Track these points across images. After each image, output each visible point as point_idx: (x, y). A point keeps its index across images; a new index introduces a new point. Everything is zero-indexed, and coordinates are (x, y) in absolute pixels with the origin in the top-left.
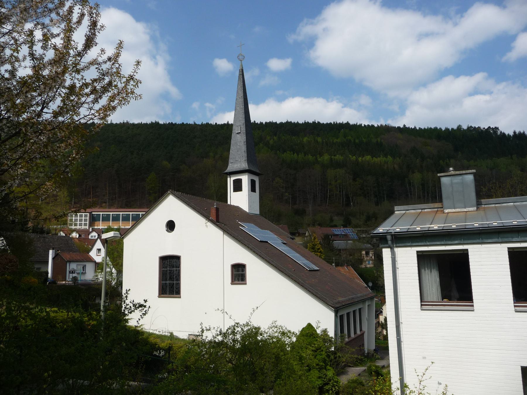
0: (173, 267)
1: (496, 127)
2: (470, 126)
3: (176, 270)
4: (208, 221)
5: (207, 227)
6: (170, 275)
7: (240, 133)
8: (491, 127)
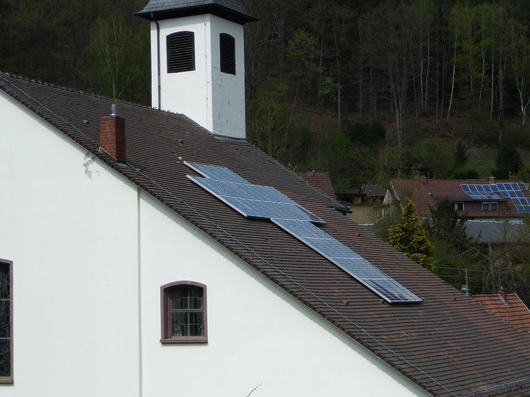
4: (93, 159)
5: (90, 177)
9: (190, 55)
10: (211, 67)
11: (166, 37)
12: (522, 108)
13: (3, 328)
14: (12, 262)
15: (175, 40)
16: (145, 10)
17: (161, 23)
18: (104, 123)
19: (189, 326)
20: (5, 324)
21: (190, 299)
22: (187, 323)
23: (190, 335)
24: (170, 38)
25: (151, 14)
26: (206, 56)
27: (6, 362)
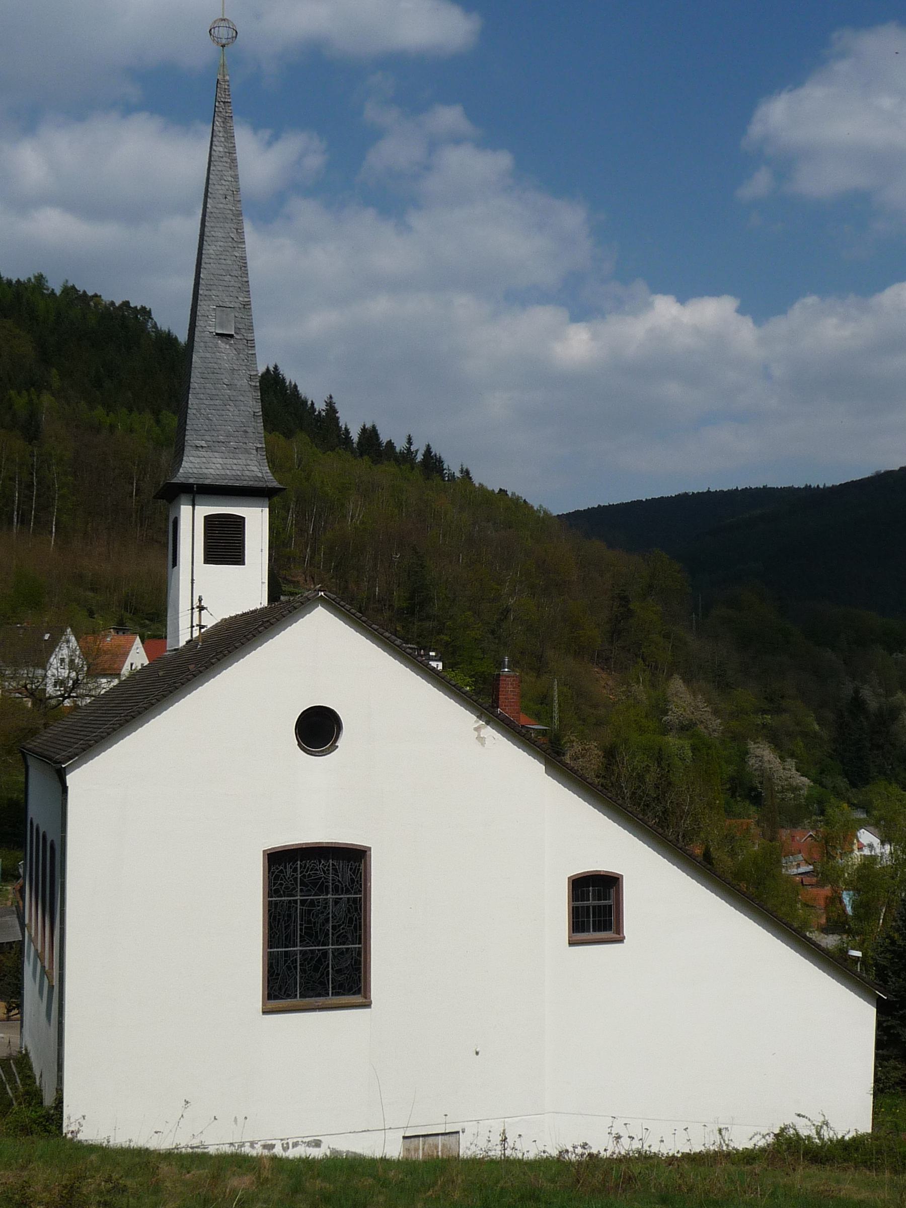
0: (323, 889)
1: (143, 308)
2: (70, 284)
3: (336, 902)
4: (488, 723)
5: (483, 744)
6: (309, 922)
7: (231, 336)
8: (132, 305)
13: (343, 933)
14: (370, 848)
17: (197, 498)
18: (505, 680)
19: (591, 922)
20: (346, 928)
21: (593, 890)
22: (590, 918)
23: (593, 931)
24: (209, 520)
27: (347, 977)
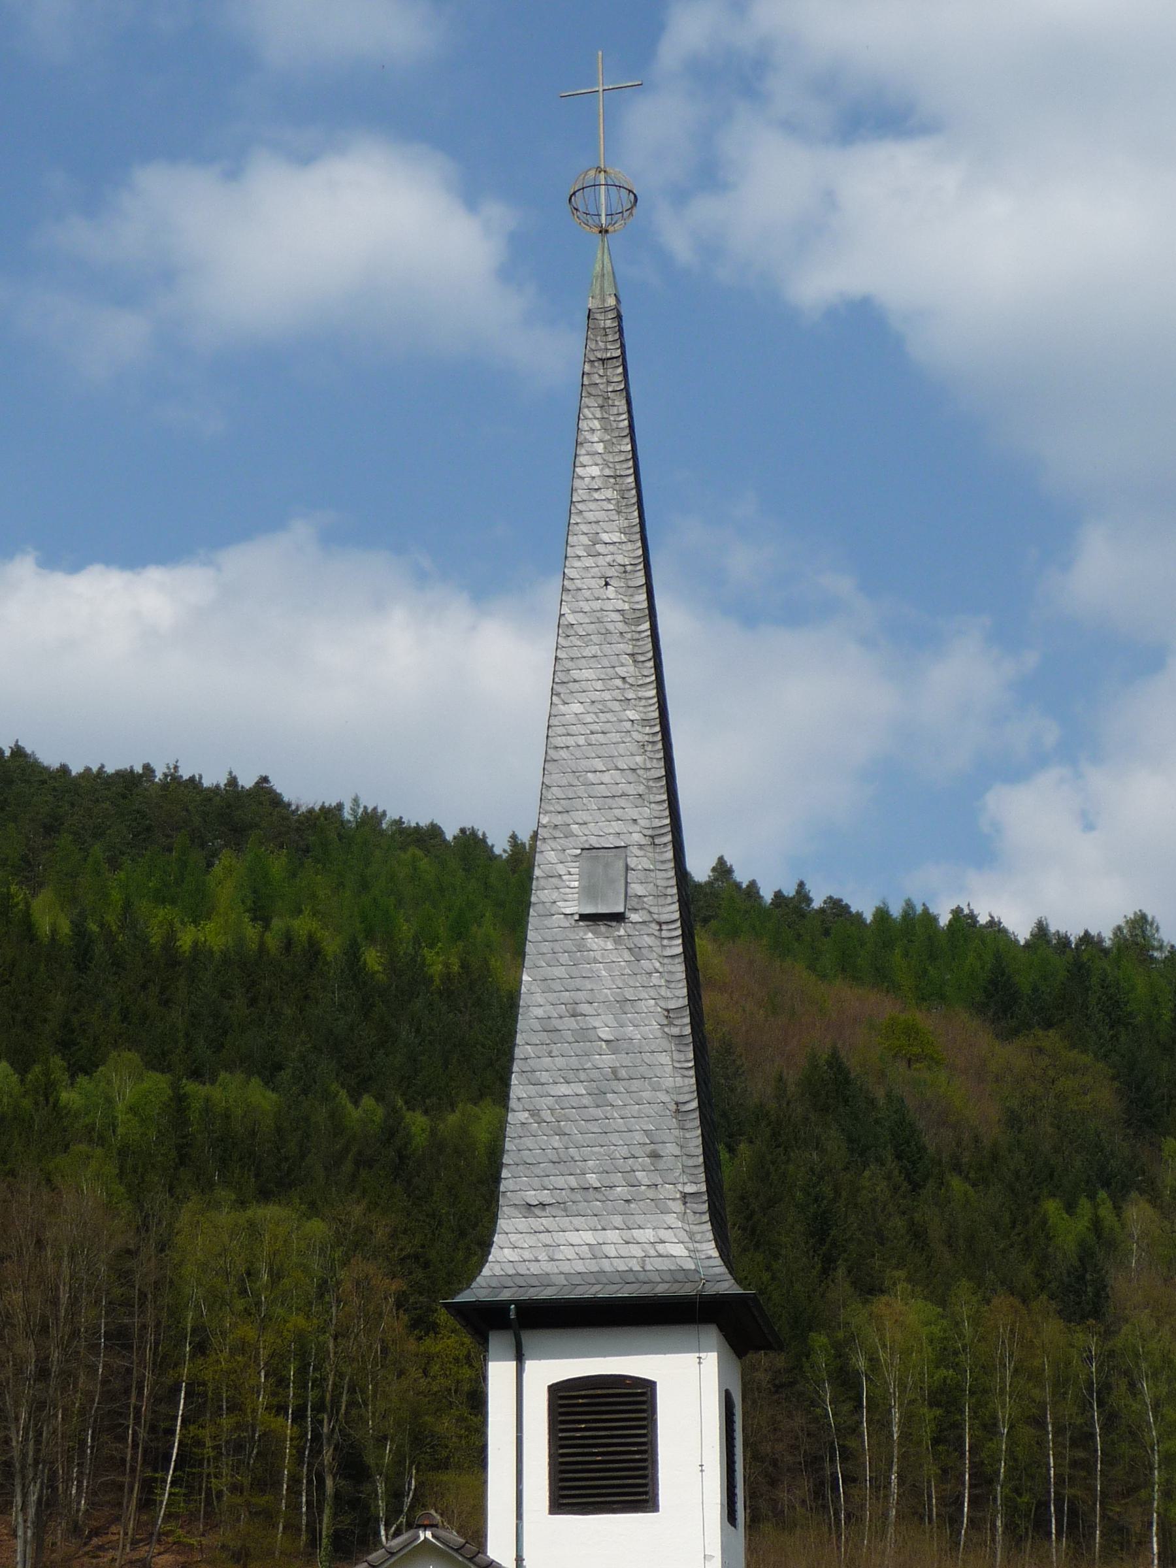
9: (637, 1457)
10: (719, 1506)
11: (546, 1388)
12: (383, 1532)
15: (581, 1401)
16: (464, 1297)
25: (509, 1310)
26: (701, 1466)
